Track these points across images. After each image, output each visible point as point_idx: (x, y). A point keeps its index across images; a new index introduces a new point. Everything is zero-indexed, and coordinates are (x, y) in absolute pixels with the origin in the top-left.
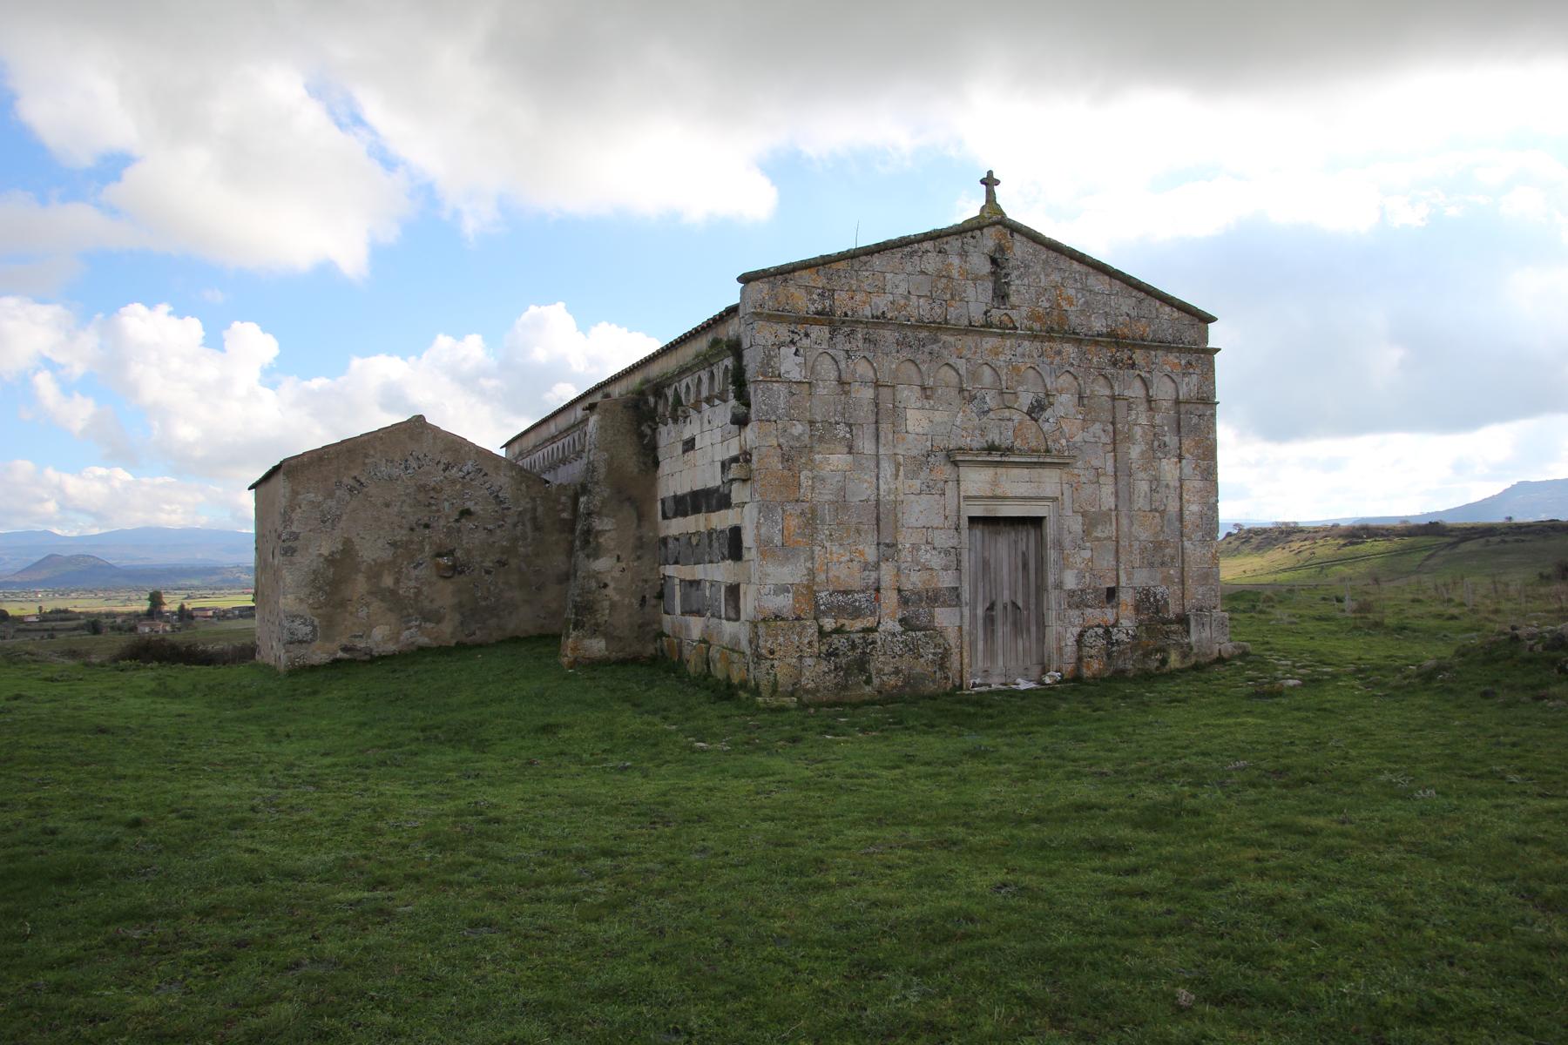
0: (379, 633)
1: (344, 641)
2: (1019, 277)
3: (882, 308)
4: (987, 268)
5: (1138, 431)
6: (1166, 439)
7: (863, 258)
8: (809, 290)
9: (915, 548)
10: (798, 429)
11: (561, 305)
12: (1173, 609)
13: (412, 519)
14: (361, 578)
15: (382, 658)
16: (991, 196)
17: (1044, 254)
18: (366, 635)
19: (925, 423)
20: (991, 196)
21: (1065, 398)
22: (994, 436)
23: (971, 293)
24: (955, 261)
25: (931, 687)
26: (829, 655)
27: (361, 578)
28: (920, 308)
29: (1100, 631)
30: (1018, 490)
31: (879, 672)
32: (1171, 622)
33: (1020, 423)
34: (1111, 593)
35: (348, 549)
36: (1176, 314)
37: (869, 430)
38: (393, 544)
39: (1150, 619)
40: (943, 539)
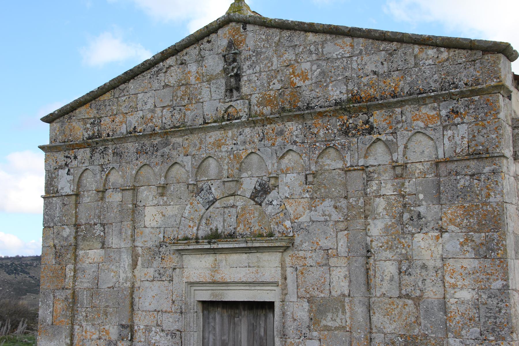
2: (250, 67)
3: (134, 123)
5: (381, 204)
6: (422, 209)
7: (122, 87)
9: (148, 329)
17: (276, 34)
19: (159, 218)
21: (290, 178)
22: (218, 225)
23: (205, 94)
24: (193, 68)
28: (165, 118)
30: (241, 275)
33: (243, 209)
36: (445, 54)
40: (170, 322)
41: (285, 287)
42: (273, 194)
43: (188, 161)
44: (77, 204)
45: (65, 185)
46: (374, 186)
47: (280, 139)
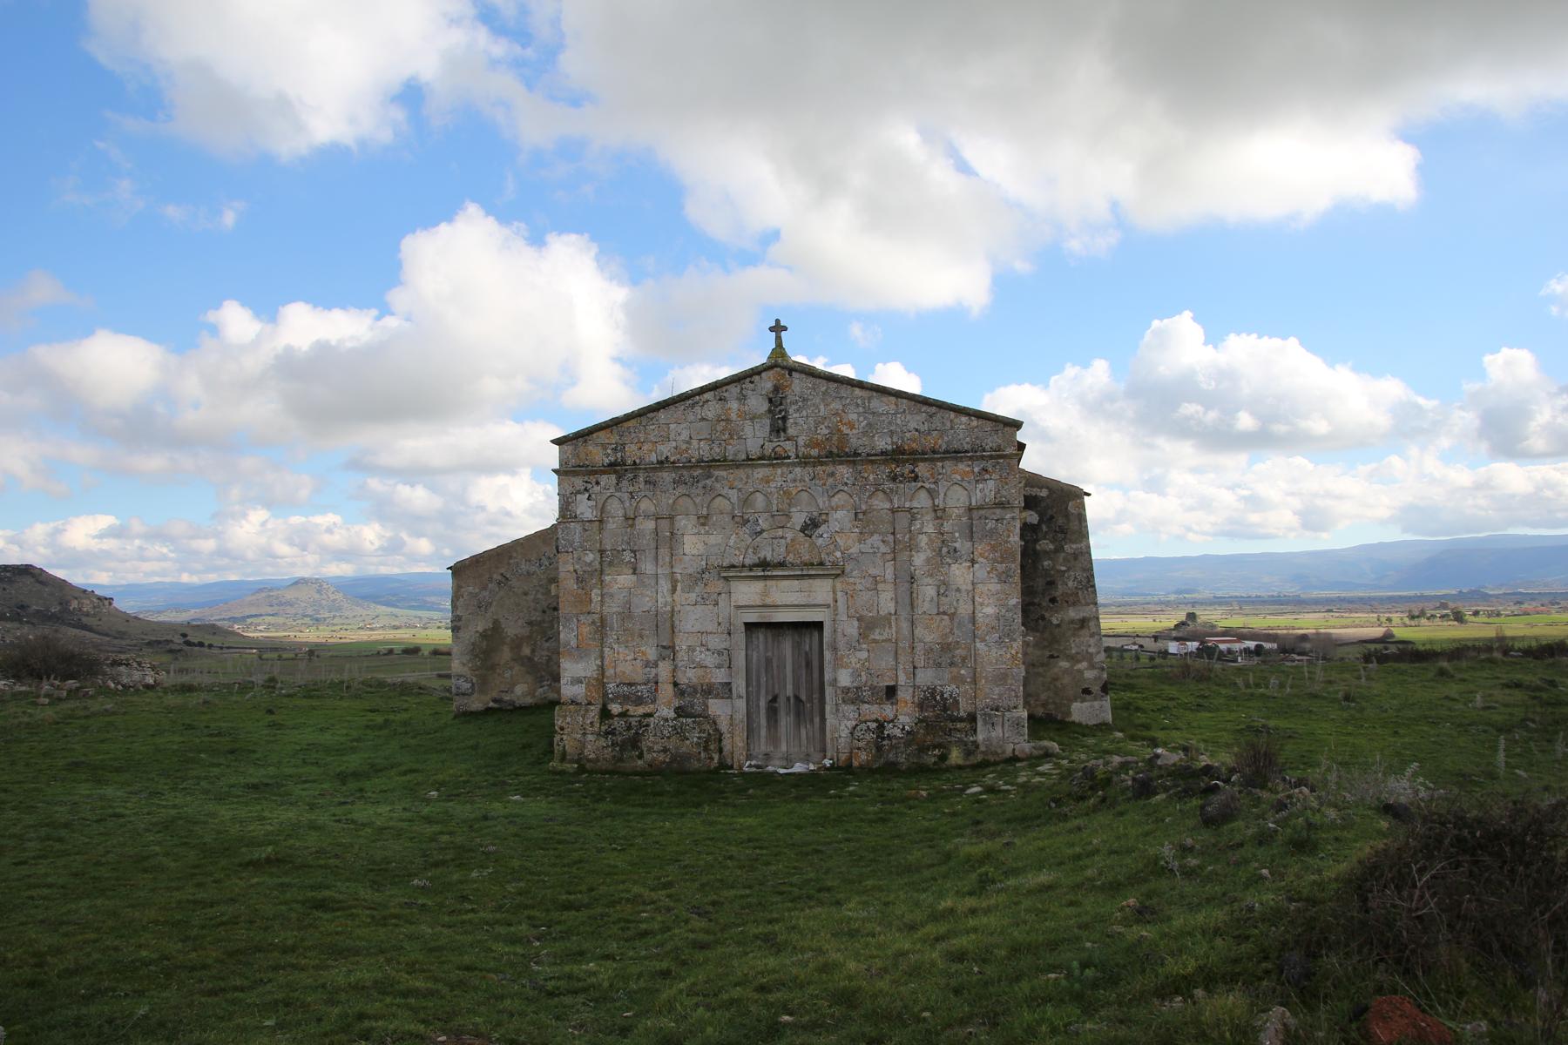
0: (520, 689)
1: (495, 694)
4: (765, 406)
5: (923, 540)
6: (957, 545)
8: (604, 447)
9: (691, 649)
10: (590, 557)
11: (1187, 314)
12: (964, 708)
13: (545, 604)
14: (506, 649)
15: (521, 708)
16: (779, 340)
17: (823, 386)
18: (510, 690)
19: (701, 546)
20: (779, 340)
21: (840, 514)
23: (748, 430)
24: (734, 405)
25: (696, 765)
26: (607, 733)
27: (506, 649)
28: (701, 449)
29: (874, 725)
30: (789, 599)
31: (650, 749)
32: (961, 720)
34: (891, 692)
35: (496, 627)
36: (975, 423)
37: (650, 555)
38: (530, 623)
39: (937, 716)
40: (716, 642)
41: (836, 609)
42: (823, 528)
43: (733, 494)
44: (601, 530)
45: (585, 508)
46: (917, 525)
47: (831, 480)
